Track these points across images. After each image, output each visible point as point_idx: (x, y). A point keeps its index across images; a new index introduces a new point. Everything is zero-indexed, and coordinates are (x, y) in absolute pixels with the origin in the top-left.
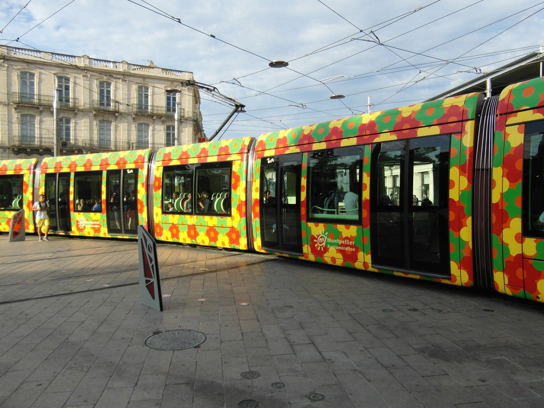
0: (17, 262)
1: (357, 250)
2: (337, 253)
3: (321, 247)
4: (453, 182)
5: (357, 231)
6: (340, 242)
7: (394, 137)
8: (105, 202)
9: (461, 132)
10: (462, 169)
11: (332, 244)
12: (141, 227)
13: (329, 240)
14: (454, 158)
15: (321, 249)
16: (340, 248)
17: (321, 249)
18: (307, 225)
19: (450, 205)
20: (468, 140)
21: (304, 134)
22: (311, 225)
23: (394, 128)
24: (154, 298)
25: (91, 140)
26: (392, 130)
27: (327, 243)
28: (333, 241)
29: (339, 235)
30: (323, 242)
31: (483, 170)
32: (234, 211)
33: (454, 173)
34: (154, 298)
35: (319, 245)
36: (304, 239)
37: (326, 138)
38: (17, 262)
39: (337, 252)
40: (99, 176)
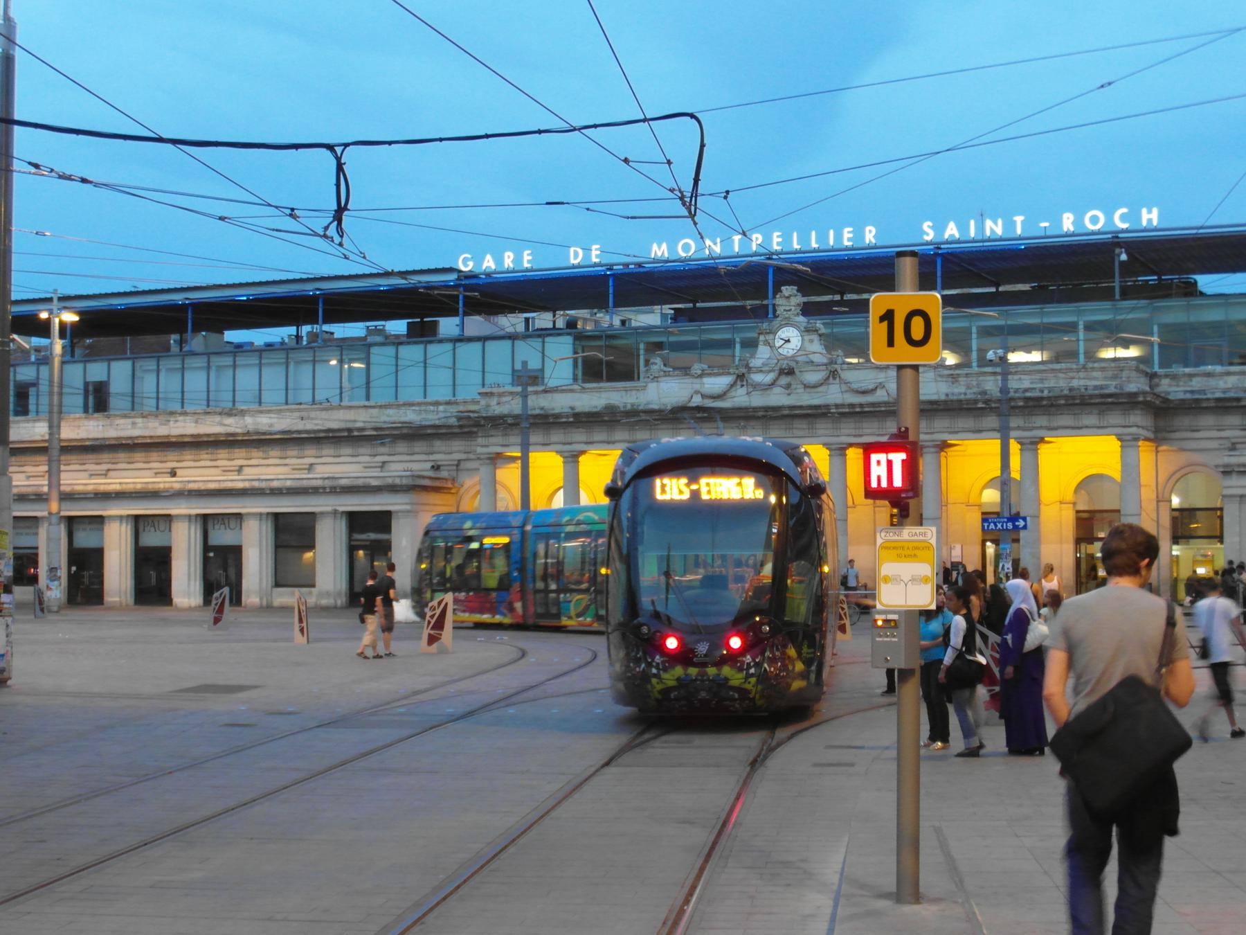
24: (446, 604)
34: (446, 604)
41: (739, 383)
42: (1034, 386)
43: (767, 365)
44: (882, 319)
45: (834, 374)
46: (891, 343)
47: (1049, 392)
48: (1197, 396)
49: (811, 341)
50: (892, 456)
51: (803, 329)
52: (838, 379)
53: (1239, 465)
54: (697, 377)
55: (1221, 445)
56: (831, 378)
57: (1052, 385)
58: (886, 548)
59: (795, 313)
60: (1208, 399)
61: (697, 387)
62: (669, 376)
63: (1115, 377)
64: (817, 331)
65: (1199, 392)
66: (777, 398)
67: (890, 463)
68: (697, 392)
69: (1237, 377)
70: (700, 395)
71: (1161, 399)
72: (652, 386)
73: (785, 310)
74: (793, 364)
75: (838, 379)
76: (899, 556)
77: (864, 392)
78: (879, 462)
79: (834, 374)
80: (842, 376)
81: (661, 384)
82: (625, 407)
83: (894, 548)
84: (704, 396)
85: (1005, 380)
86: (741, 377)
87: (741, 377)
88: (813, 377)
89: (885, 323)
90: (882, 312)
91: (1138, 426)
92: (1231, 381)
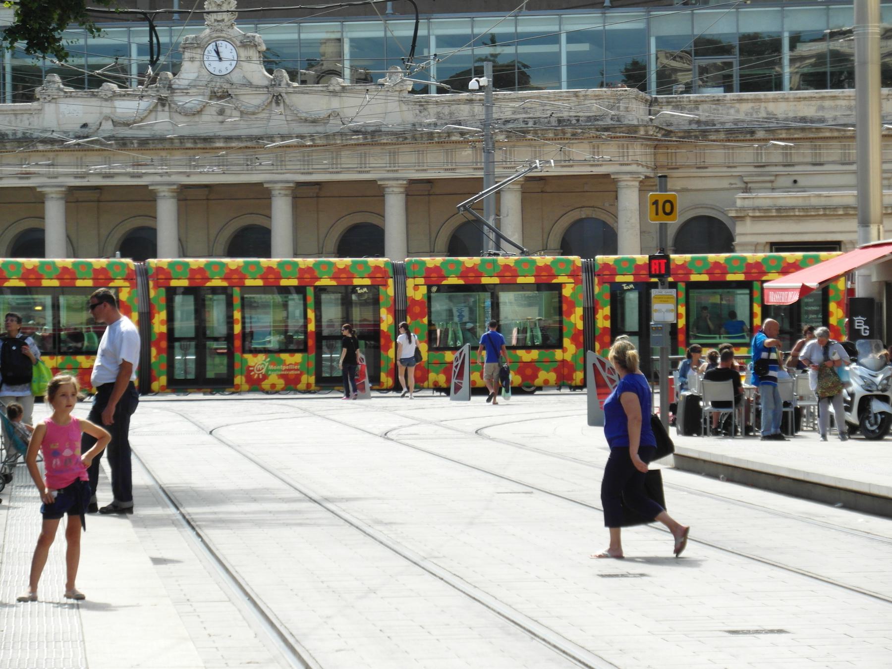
0: (530, 618)
1: (301, 374)
2: (548, 373)
3: (259, 374)
4: (756, 313)
5: (303, 358)
6: (284, 368)
7: (334, 283)
8: (314, 336)
9: (386, 285)
10: (389, 310)
11: (273, 370)
12: (127, 385)
13: (271, 367)
14: (832, 296)
15: (259, 376)
16: (283, 373)
17: (259, 376)
18: (242, 357)
19: (381, 334)
20: (391, 291)
21: (677, 265)
22: (248, 356)
23: (571, 273)
25: (401, 193)
26: (569, 274)
27: (267, 370)
28: (275, 368)
29: (283, 362)
30: (262, 369)
31: (588, 308)
32: (567, 342)
33: (833, 307)
35: (255, 370)
36: (237, 370)
37: (369, 275)
38: (530, 618)
39: (279, 378)
40: (486, 286)
41: (160, 108)
42: (518, 116)
43: (195, 86)
44: (654, 204)
45: (277, 99)
46: (657, 214)
47: (535, 123)
48: (704, 127)
49: (249, 60)
50: (661, 261)
51: (238, 43)
52: (282, 105)
53: (754, 209)
54: (106, 100)
55: (731, 184)
56: (274, 104)
57: (538, 115)
58: (656, 298)
59: (229, 23)
60: (717, 131)
61: (107, 111)
62: (71, 97)
63: (612, 107)
64: (256, 46)
65: (706, 123)
66: (207, 124)
67: (660, 263)
68: (107, 118)
69: (750, 105)
70: (110, 123)
71: (663, 132)
72: (49, 108)
73: (216, 21)
74: (226, 86)
75: (282, 105)
76: (661, 301)
77: (314, 122)
78: (655, 263)
79: (277, 99)
80: (287, 101)
81: (61, 105)
82: (15, 134)
83: (659, 298)
84: (115, 123)
85: (488, 109)
86: (162, 101)
87: (162, 101)
88: (253, 100)
89: (655, 206)
90: (653, 201)
91: (638, 165)
92: (745, 107)
